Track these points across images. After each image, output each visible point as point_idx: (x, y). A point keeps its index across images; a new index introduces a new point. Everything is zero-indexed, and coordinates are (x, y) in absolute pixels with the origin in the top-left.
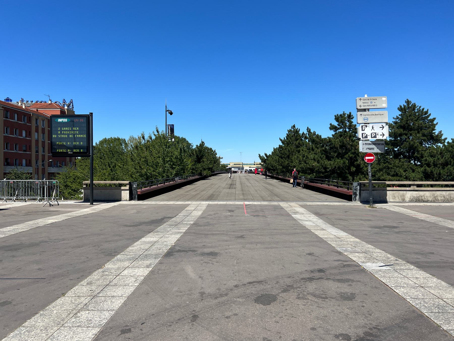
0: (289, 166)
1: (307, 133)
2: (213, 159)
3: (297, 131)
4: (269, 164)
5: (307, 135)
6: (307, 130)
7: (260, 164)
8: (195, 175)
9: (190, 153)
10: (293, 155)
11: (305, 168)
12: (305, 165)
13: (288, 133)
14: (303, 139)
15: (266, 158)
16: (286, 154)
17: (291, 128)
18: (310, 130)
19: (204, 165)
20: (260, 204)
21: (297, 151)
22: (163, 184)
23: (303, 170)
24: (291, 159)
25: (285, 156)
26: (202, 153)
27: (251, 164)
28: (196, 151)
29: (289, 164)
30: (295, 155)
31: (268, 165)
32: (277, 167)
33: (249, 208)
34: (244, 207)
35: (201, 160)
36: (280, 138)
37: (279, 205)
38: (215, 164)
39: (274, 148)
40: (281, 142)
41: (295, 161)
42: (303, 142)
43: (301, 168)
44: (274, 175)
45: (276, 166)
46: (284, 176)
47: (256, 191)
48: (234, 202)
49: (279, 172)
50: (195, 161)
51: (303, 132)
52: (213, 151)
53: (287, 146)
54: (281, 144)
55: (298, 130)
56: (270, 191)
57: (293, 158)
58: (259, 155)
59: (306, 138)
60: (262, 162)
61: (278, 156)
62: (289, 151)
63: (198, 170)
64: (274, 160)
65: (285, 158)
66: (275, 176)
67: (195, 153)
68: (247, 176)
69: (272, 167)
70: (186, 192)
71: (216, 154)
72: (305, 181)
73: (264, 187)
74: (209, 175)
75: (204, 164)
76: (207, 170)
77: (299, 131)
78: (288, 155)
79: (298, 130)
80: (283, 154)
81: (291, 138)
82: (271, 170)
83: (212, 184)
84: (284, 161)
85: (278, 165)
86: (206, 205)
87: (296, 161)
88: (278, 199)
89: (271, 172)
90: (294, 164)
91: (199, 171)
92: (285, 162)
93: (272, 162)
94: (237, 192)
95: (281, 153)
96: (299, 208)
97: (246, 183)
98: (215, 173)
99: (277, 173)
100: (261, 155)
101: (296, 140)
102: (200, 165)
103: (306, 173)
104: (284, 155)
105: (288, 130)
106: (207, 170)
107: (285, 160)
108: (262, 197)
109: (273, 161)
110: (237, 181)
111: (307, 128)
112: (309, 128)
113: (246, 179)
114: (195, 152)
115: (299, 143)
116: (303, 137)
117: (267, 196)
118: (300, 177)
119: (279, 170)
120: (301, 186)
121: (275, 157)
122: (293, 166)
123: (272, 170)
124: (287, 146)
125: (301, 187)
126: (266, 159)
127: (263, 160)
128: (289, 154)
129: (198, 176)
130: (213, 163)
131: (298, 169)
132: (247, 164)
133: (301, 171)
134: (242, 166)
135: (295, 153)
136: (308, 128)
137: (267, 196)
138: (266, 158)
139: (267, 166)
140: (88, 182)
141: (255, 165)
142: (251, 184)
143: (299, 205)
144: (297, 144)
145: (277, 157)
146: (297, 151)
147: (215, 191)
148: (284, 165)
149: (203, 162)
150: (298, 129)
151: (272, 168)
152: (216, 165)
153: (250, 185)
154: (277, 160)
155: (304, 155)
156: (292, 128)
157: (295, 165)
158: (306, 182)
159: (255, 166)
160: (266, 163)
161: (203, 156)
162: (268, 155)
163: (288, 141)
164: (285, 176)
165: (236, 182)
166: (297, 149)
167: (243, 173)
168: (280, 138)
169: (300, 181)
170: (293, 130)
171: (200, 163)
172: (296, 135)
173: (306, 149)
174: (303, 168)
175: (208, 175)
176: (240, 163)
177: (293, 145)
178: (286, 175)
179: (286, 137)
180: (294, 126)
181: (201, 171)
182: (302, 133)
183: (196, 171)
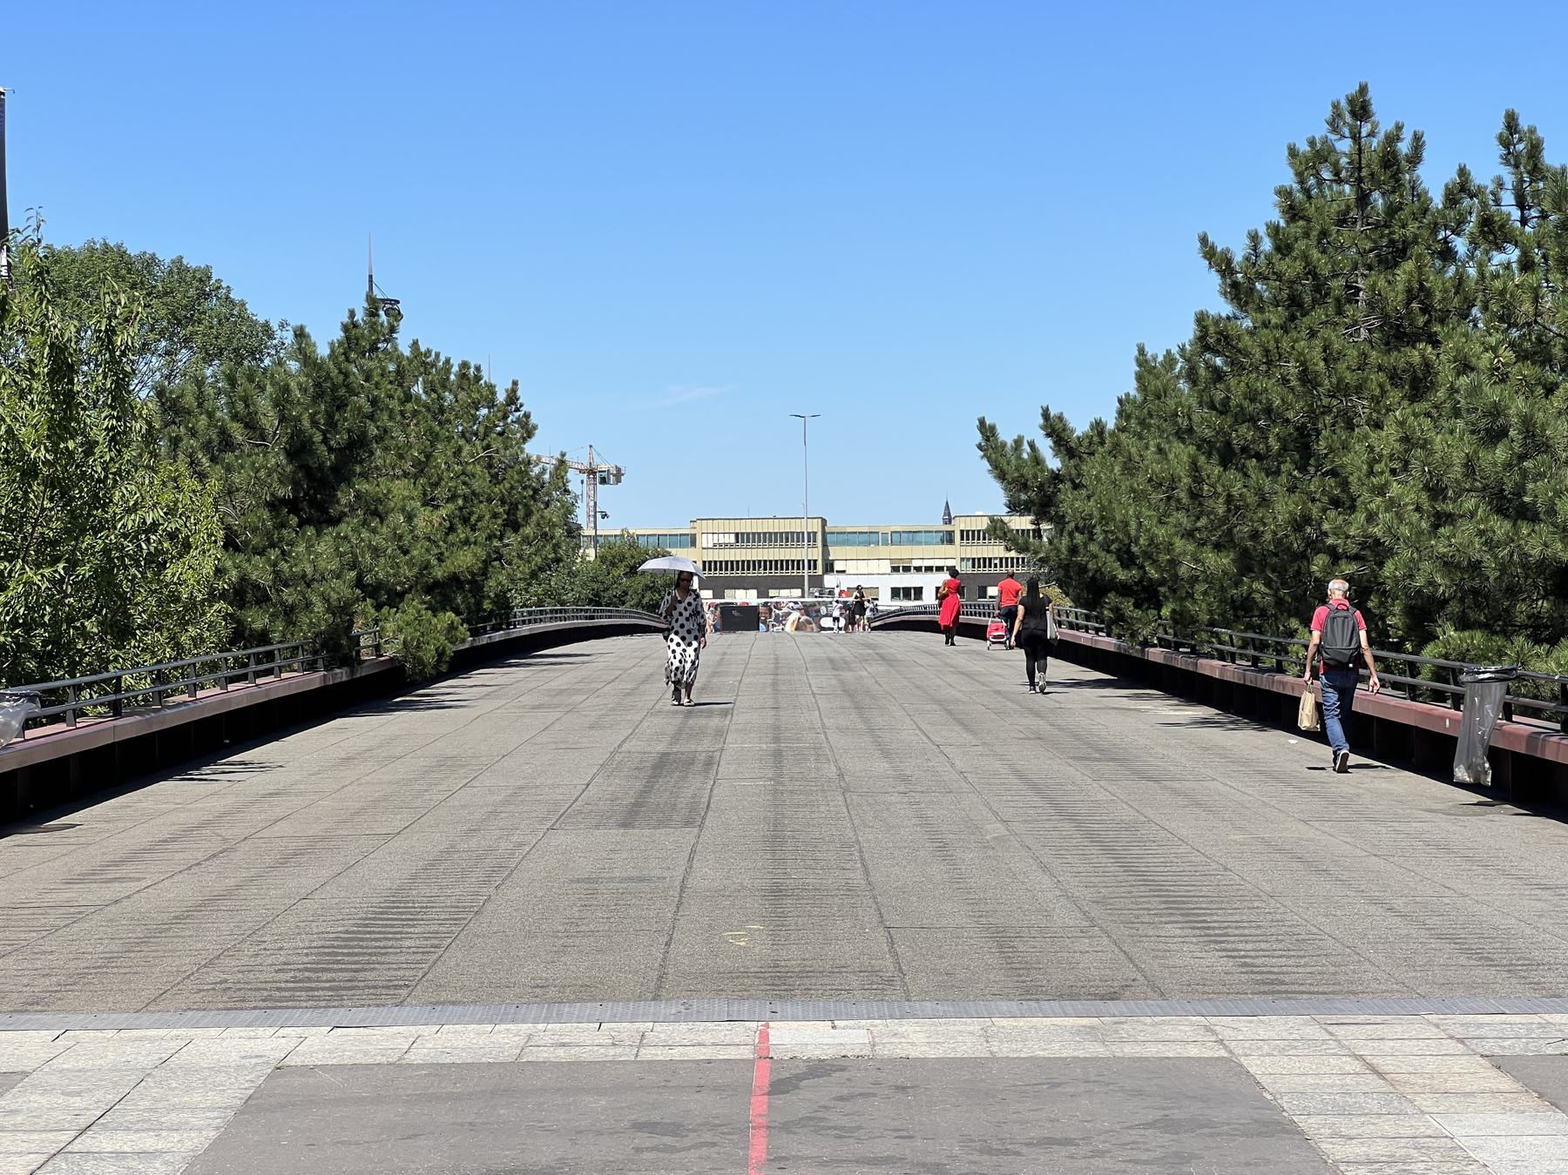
0: (1314, 546)
1: (1509, 179)
2: (496, 480)
3: (1389, 160)
4: (1089, 531)
5: (1508, 198)
6: (1506, 143)
7: (997, 530)
8: (270, 656)
9: (223, 414)
10: (1350, 427)
11: (1503, 568)
12: (1501, 527)
13: (1289, 179)
14: (1460, 245)
15: (1054, 463)
16: (1268, 411)
17: (1321, 131)
18: (1535, 149)
19: (376, 552)
20: (981, 1051)
21: (1394, 377)
22: (61, 727)
23: (1475, 592)
24: (1333, 473)
25: (1263, 434)
26: (347, 419)
27: (911, 537)
28: (286, 389)
29: (1307, 520)
30: (1378, 426)
31: (1079, 538)
32: (1174, 563)
33: (814, 1123)
34: (759, 1106)
35: (345, 497)
36: (1204, 240)
37: (1232, 1066)
38: (512, 539)
39: (1142, 359)
40: (1215, 279)
41: (1381, 490)
42: (1460, 280)
43: (1448, 565)
44: (1146, 644)
45: (1169, 547)
46: (1255, 661)
47: (943, 850)
48: (626, 1030)
49: (1200, 609)
50: (274, 505)
51: (1463, 172)
52: (491, 404)
53: (1284, 328)
54: (1222, 307)
55: (1404, 147)
56: (1108, 849)
57: (1354, 461)
58: (987, 430)
59: (1493, 232)
60: (1015, 507)
61: (1185, 434)
62: (1307, 378)
63: (308, 605)
64: (1140, 482)
65: (1259, 457)
66: (1156, 654)
67: (269, 419)
68: (865, 660)
69: (1127, 559)
70: (81, 879)
71: (528, 432)
72: (1508, 711)
73: (1036, 788)
74: (440, 654)
75: (377, 540)
76: (414, 606)
77: (1415, 158)
78: (1301, 429)
79: (1404, 147)
80: (1243, 417)
81: (1324, 234)
82: (1112, 599)
83: (448, 764)
84: (1260, 492)
85: (1189, 535)
86: (234, 1093)
87: (1395, 489)
88: (1213, 962)
89: (1116, 610)
90: (1371, 517)
91: (318, 617)
92: (1264, 501)
93: (1125, 510)
94: (707, 875)
95: (1223, 409)
96: (1511, 1120)
97: (834, 738)
98: (524, 630)
99: (1182, 620)
100: (1006, 436)
101: (1381, 260)
102: (324, 546)
103: (1500, 624)
104: (1253, 420)
105: (1293, 153)
106: (414, 606)
107: (1267, 484)
108: (1001, 938)
109: (1139, 496)
110: (739, 719)
111: (1500, 127)
112: (1524, 124)
113: (848, 693)
114: (276, 404)
115: (1419, 293)
116: (1461, 222)
117: (1065, 916)
118: (1440, 674)
119: (1201, 587)
120: (1461, 773)
121: (1160, 450)
122: (1353, 549)
123: (1124, 590)
124: (1284, 328)
125: (1462, 785)
126: (1056, 477)
127: (1025, 487)
128: (1313, 415)
129: (311, 667)
130: (496, 526)
131: (1420, 582)
132: (869, 538)
133: (1454, 607)
134: (816, 554)
135: (1376, 400)
136: (1511, 123)
137: (1065, 916)
138: (1054, 463)
139: (1073, 550)
140: (553, 555)
141: (949, 538)
142: (886, 754)
143: (1499, 1063)
144: (1395, 298)
145: (1181, 453)
146: (1394, 377)
147: (451, 850)
148: (1255, 535)
149: (375, 510)
150: (1407, 135)
151: (1122, 575)
152: (526, 540)
153: (882, 766)
154: (1174, 480)
155: (1496, 411)
156: (1334, 126)
157: (1377, 531)
158: (1523, 725)
159: (955, 555)
160: (1059, 521)
161: (358, 445)
162: (1079, 426)
163: (1299, 266)
164: (1269, 660)
165: (720, 733)
166: (1398, 359)
167: (826, 622)
168: (1204, 240)
169: (1443, 710)
170: (1345, 146)
171: (335, 522)
172: (1378, 200)
173: (1507, 355)
174: (1476, 566)
175: (429, 656)
176: (795, 527)
177: (1349, 310)
178: (1281, 650)
179: (1274, 231)
180: (1360, 108)
181: (344, 611)
182: (1452, 176)
183: (289, 612)
